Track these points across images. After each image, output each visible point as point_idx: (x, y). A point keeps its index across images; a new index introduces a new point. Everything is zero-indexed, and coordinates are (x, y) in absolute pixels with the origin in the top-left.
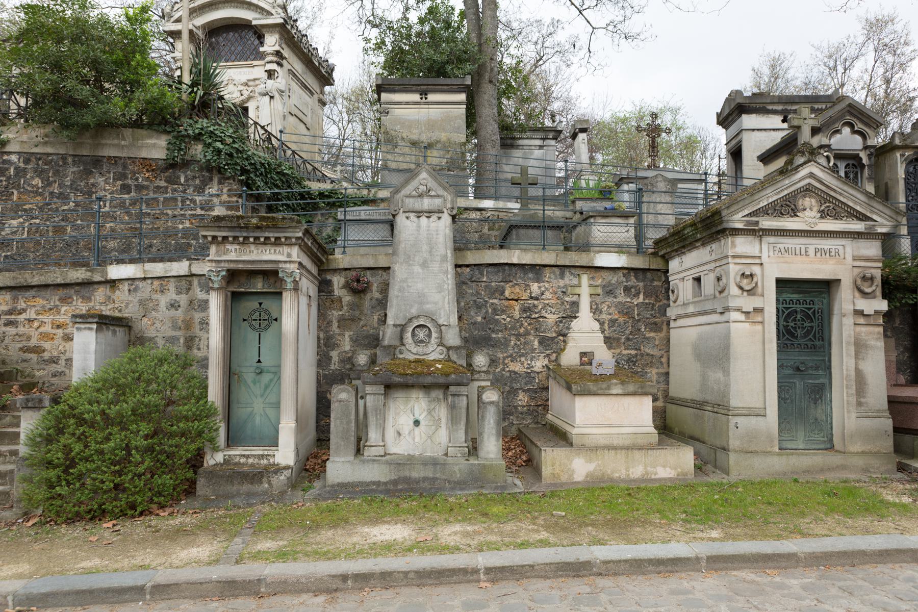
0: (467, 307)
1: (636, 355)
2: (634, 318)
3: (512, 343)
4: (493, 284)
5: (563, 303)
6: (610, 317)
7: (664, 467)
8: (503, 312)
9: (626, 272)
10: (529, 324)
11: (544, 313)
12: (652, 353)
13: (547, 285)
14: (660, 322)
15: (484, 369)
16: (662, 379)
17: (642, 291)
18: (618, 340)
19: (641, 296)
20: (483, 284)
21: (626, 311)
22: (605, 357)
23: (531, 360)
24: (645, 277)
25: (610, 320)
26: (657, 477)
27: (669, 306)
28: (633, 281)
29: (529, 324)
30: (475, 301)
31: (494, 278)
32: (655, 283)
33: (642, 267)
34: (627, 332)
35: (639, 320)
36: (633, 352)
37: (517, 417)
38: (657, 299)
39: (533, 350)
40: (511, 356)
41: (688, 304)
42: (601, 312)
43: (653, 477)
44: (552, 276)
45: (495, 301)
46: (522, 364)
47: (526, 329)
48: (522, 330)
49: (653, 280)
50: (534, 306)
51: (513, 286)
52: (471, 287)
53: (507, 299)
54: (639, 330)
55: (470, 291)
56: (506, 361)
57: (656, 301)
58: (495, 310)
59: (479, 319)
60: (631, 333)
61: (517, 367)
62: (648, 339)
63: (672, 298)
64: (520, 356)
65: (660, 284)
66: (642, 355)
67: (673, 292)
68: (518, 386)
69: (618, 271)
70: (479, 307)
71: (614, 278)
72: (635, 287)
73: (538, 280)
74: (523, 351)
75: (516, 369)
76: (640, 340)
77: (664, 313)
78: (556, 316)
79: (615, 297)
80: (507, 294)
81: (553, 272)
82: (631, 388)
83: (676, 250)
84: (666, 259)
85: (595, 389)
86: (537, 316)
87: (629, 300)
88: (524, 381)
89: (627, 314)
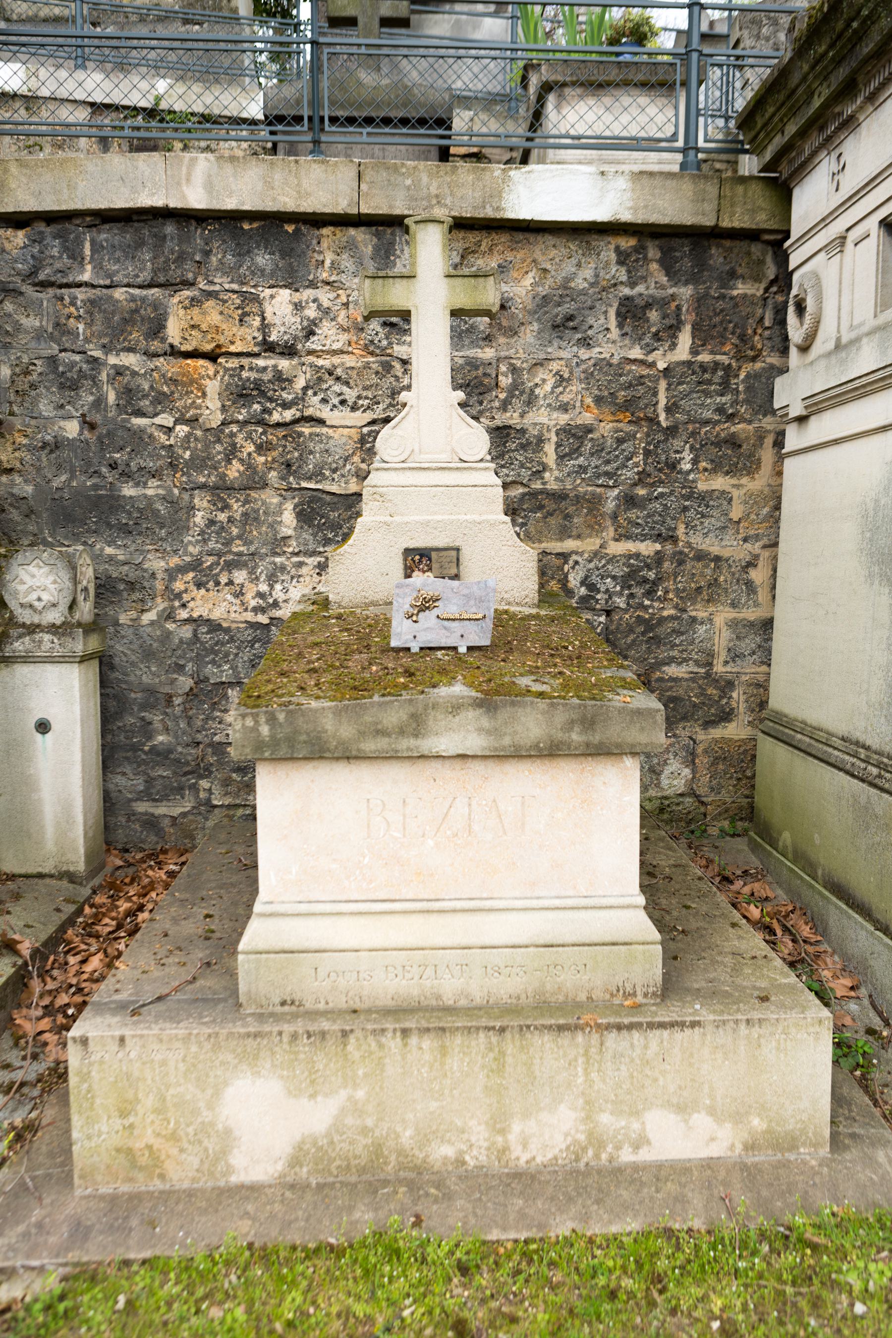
0: (23, 383)
1: (659, 558)
2: (653, 421)
3: (199, 518)
4: (119, 294)
5: (387, 367)
6: (563, 419)
7: (683, 1109)
8: (162, 401)
9: (627, 243)
10: (261, 449)
11: (314, 406)
12: (715, 550)
13: (325, 296)
14: (742, 427)
15: (55, 617)
16: (749, 643)
17: (688, 318)
18: (595, 502)
19: (685, 339)
20: (81, 294)
21: (624, 395)
22: (504, 568)
23: (272, 579)
24: (701, 264)
25: (566, 431)
26: (645, 1155)
27: (783, 370)
28: (655, 282)
29: (261, 449)
30: (52, 361)
31: (124, 271)
32: (741, 289)
33: (687, 218)
34: (628, 474)
35: (672, 431)
36: (647, 548)
37: (226, 782)
38: (745, 352)
39: (278, 544)
40: (195, 565)
41: (856, 341)
42: (531, 401)
43: (626, 1156)
44: (346, 262)
45: (130, 360)
46: (239, 594)
47: (250, 466)
48: (234, 471)
49: (732, 275)
50: (280, 378)
51: (194, 302)
52: (28, 307)
53: (174, 352)
54: (673, 466)
55: (30, 322)
56: (178, 586)
57: (740, 357)
58: (128, 394)
59: (72, 429)
60: (642, 478)
61: (216, 605)
62: (704, 498)
63: (796, 331)
64: (230, 566)
65: (754, 290)
66: (680, 559)
67: (801, 309)
68: (226, 673)
69: (599, 242)
70: (70, 385)
71: (582, 270)
72: (662, 303)
73: (292, 278)
74: (238, 547)
75: (217, 614)
76: (672, 503)
77: (764, 403)
78: (360, 418)
79: (586, 343)
80: (173, 331)
81: (351, 246)
82: (531, 724)
83: (817, 122)
84: (781, 188)
85: (347, 731)
86: (288, 415)
87: (636, 353)
88: (246, 655)
89: (628, 405)
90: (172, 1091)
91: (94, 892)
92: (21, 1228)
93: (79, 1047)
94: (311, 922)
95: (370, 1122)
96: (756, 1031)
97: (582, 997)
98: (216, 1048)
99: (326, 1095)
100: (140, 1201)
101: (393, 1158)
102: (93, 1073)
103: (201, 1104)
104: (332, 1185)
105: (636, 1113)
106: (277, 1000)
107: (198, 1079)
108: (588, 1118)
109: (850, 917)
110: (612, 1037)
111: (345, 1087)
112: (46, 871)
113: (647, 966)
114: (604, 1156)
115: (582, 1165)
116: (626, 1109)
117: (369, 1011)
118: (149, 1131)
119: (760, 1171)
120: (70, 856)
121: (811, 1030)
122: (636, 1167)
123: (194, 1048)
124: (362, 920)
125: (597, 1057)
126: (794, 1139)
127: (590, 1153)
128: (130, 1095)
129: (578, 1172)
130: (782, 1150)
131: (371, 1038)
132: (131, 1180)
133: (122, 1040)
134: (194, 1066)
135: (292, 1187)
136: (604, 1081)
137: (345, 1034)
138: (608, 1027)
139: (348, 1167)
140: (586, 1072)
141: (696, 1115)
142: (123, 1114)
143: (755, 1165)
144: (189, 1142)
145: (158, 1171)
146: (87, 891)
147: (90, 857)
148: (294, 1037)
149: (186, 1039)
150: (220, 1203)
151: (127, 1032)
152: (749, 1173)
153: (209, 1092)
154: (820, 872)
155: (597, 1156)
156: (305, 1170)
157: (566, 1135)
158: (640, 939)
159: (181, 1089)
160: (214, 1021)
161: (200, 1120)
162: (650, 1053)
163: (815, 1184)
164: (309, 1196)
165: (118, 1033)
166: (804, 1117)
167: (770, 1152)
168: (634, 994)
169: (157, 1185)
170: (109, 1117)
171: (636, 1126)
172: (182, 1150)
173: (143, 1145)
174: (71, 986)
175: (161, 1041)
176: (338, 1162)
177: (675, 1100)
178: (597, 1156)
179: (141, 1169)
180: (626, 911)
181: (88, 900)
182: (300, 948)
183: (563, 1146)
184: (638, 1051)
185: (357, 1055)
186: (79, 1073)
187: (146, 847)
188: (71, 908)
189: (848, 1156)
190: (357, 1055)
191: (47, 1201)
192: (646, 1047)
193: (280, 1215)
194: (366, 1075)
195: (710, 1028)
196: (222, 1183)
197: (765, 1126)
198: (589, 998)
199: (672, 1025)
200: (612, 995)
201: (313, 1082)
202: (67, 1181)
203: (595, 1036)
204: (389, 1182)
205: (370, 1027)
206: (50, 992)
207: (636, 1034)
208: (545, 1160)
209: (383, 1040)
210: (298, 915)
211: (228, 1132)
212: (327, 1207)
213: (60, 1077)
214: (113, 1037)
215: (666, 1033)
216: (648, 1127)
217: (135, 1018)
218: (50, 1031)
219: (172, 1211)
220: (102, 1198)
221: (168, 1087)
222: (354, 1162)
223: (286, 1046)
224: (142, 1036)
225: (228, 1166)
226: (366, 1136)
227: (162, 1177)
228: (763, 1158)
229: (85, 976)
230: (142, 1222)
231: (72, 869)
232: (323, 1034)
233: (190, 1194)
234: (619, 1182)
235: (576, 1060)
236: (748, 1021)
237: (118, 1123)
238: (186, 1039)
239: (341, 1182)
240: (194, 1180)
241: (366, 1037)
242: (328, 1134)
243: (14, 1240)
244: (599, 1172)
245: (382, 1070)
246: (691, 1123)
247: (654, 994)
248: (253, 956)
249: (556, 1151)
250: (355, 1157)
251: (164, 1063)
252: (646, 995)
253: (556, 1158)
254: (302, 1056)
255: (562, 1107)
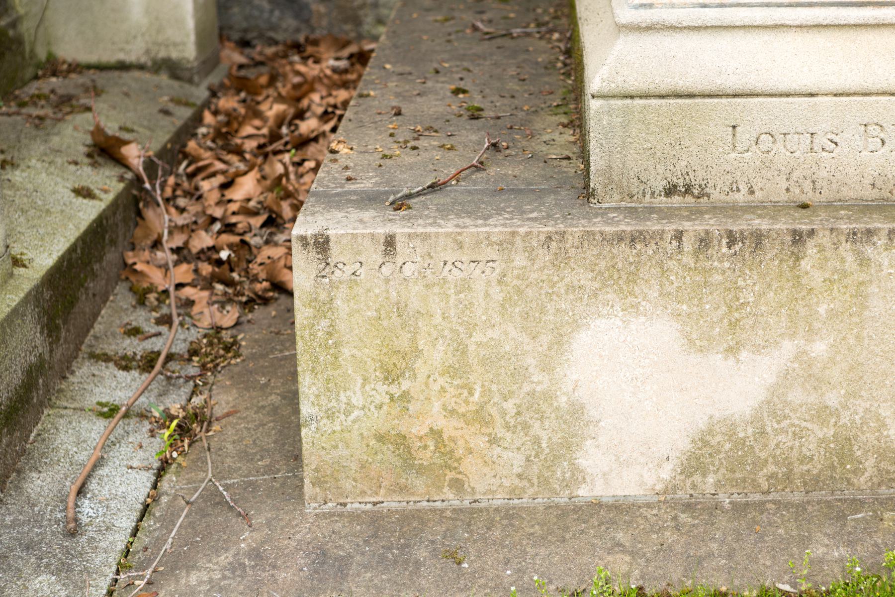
90: (478, 337)
91: (214, 94)
92: (224, 559)
93: (313, 255)
94: (724, 41)
95: (832, 399)
98: (561, 260)
99: (757, 349)
100: (423, 522)
101: (870, 463)
102: (338, 302)
103: (530, 361)
104: (760, 506)
106: (660, 185)
107: (526, 316)
111: (793, 336)
112: (131, 58)
117: (829, 206)
118: (437, 406)
120: (171, 34)
123: (520, 260)
124: (820, 39)
128: (403, 342)
131: (846, 247)
132: (402, 489)
133: (390, 243)
134: (519, 292)
135: (688, 507)
137: (798, 238)
139: (788, 477)
142: (390, 376)
144: (507, 427)
145: (450, 475)
146: (201, 93)
147: (201, 43)
148: (705, 242)
149: (506, 244)
150: (566, 529)
151: (399, 229)
153: (545, 339)
156: (711, 479)
159: (494, 333)
160: (549, 216)
161: (527, 388)
164: (722, 521)
165: (382, 231)
169: (450, 498)
170: (365, 380)
172: (493, 441)
173: (425, 430)
174: (213, 220)
175: (460, 245)
176: (771, 468)
179: (421, 470)
181: (206, 105)
182: (706, 87)
185: (817, 277)
186: (313, 301)
187: (279, 37)
188: (184, 114)
190: (817, 277)
191: (259, 520)
193: (678, 548)
194: (832, 314)
196: (563, 500)
201: (733, 325)
202: (293, 491)
204: (862, 503)
205: (844, 226)
206: (182, 228)
209: (869, 250)
210: (698, 28)
211: (577, 410)
212: (761, 538)
213: (227, 349)
214: (373, 236)
217: (402, 213)
218: (193, 285)
219: (484, 539)
220: (355, 517)
221: (471, 328)
222: (798, 469)
223: (688, 260)
224: (425, 237)
225: (575, 469)
226: (824, 423)
227: (457, 485)
229: (234, 207)
230: (435, 553)
231: (174, 55)
232: (758, 238)
233: (510, 515)
237: (381, 391)
238: (506, 244)
239: (774, 502)
240: (513, 492)
241: (836, 246)
242: (756, 419)
243: (217, 576)
245: (864, 307)
248: (620, 102)
250: (803, 460)
251: (465, 286)
254: (717, 278)
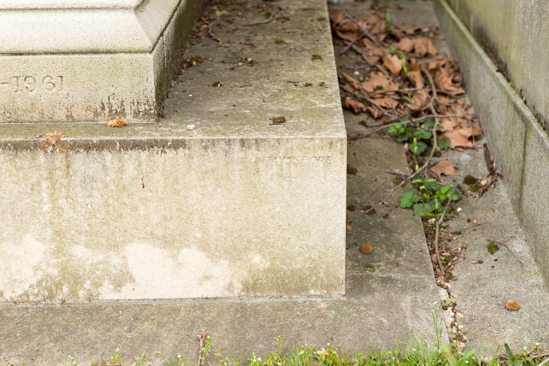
7: (170, 242)
26: (128, 293)
43: (107, 294)
96: (252, 154)
97: (61, 115)
105: (116, 247)
108: (59, 250)
109: (482, 62)
110: (79, 159)
113: (137, 80)
114: (81, 293)
115: (57, 302)
116: (103, 241)
119: (257, 313)
121: (321, 153)
122: (118, 306)
125: (65, 181)
126: (302, 279)
127: (66, 289)
129: (51, 309)
130: (288, 291)
136: (74, 209)
138: (74, 147)
140: (53, 200)
141: (185, 250)
143: (254, 307)
152: (242, 313)
154: (472, 19)
155: (74, 293)
157: (36, 269)
158: (126, 46)
162: (126, 178)
163: (313, 327)
166: (314, 254)
167: (274, 293)
168: (123, 113)
171: (115, 260)
177: (160, 233)
178: (74, 293)
180: (112, 14)
183: (34, 281)
184: (112, 175)
189: (367, 299)
192: (121, 171)
195: (197, 150)
197: (268, 265)
198: (70, 117)
199: (151, 145)
200: (96, 114)
203: (59, 158)
207: (108, 155)
208: (15, 296)
215: (144, 155)
216: (130, 262)
228: (266, 300)
234: (92, 321)
235: (39, 185)
236: (243, 142)
244: (74, 310)
246: (180, 258)
247: (146, 113)
249: (26, 286)
252: (136, 114)
253: (26, 294)
255: (28, 238)
